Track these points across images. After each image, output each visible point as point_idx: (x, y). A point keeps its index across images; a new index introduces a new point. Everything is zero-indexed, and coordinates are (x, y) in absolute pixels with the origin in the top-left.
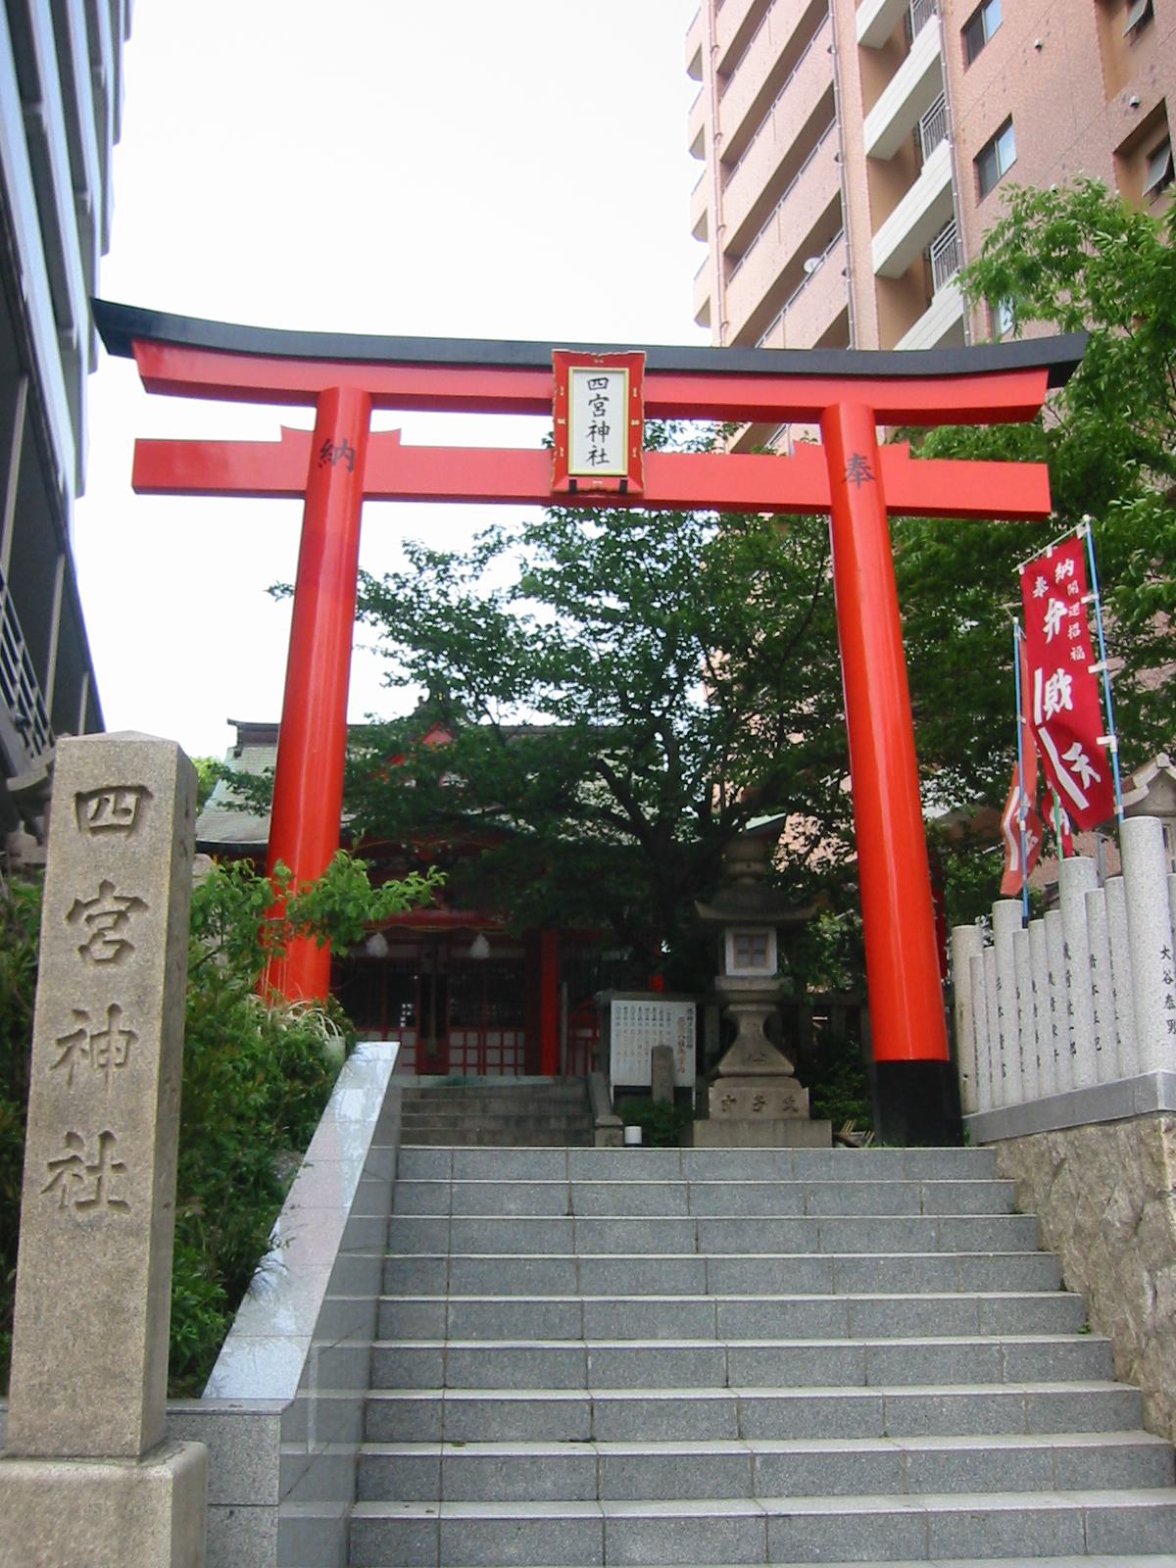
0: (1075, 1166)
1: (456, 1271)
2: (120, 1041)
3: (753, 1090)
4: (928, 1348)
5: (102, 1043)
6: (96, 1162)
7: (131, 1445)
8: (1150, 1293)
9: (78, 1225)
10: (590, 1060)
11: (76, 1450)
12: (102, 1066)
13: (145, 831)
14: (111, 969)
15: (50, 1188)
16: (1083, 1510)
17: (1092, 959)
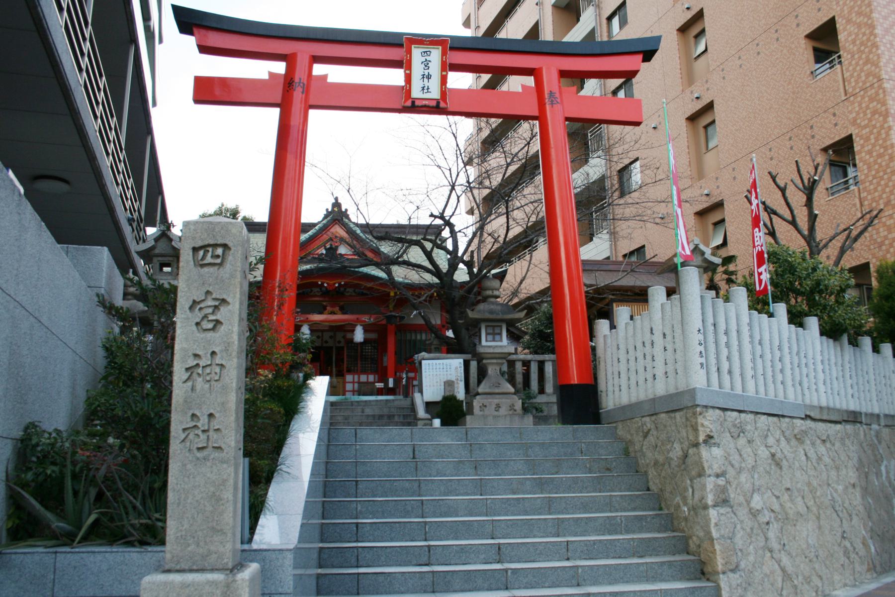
0: (655, 433)
1: (360, 486)
2: (217, 370)
3: (496, 400)
4: (587, 518)
5: (208, 370)
6: (206, 428)
7: (227, 564)
8: (690, 490)
9: (198, 459)
10: (500, 361)
11: (199, 567)
12: (208, 381)
13: (228, 266)
14: (210, 334)
15: (183, 441)
16: (661, 590)
17: (664, 335)
